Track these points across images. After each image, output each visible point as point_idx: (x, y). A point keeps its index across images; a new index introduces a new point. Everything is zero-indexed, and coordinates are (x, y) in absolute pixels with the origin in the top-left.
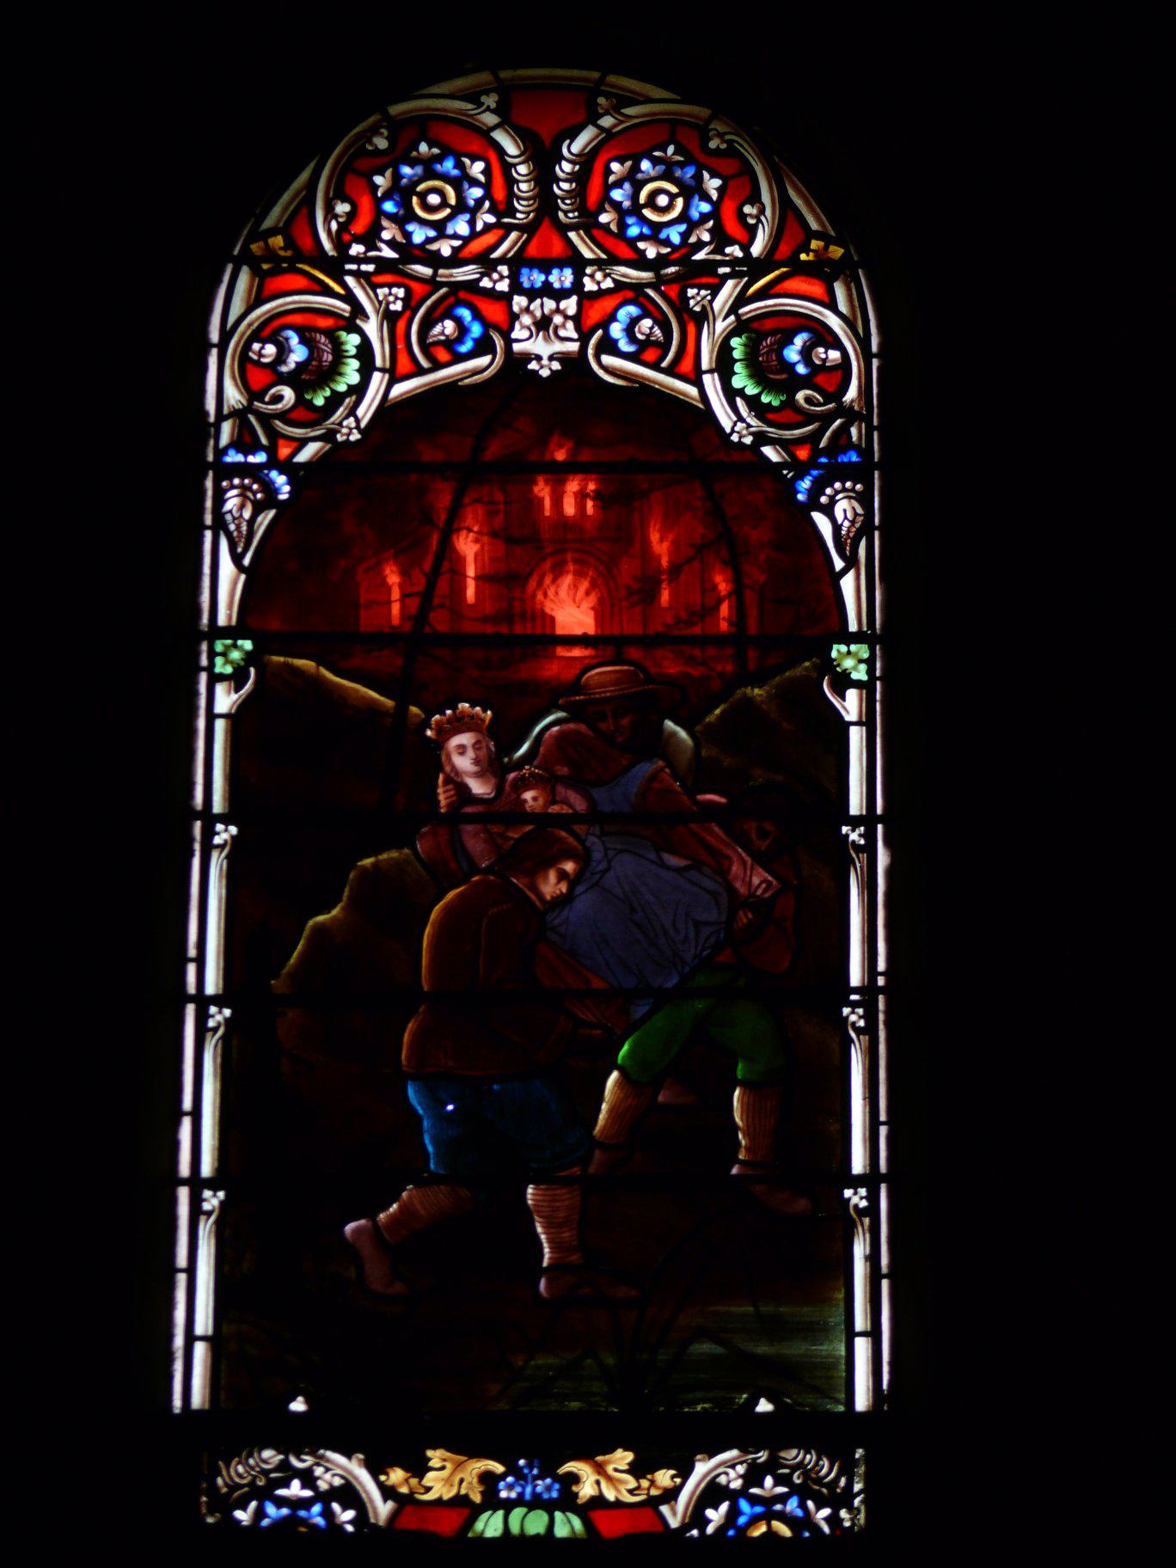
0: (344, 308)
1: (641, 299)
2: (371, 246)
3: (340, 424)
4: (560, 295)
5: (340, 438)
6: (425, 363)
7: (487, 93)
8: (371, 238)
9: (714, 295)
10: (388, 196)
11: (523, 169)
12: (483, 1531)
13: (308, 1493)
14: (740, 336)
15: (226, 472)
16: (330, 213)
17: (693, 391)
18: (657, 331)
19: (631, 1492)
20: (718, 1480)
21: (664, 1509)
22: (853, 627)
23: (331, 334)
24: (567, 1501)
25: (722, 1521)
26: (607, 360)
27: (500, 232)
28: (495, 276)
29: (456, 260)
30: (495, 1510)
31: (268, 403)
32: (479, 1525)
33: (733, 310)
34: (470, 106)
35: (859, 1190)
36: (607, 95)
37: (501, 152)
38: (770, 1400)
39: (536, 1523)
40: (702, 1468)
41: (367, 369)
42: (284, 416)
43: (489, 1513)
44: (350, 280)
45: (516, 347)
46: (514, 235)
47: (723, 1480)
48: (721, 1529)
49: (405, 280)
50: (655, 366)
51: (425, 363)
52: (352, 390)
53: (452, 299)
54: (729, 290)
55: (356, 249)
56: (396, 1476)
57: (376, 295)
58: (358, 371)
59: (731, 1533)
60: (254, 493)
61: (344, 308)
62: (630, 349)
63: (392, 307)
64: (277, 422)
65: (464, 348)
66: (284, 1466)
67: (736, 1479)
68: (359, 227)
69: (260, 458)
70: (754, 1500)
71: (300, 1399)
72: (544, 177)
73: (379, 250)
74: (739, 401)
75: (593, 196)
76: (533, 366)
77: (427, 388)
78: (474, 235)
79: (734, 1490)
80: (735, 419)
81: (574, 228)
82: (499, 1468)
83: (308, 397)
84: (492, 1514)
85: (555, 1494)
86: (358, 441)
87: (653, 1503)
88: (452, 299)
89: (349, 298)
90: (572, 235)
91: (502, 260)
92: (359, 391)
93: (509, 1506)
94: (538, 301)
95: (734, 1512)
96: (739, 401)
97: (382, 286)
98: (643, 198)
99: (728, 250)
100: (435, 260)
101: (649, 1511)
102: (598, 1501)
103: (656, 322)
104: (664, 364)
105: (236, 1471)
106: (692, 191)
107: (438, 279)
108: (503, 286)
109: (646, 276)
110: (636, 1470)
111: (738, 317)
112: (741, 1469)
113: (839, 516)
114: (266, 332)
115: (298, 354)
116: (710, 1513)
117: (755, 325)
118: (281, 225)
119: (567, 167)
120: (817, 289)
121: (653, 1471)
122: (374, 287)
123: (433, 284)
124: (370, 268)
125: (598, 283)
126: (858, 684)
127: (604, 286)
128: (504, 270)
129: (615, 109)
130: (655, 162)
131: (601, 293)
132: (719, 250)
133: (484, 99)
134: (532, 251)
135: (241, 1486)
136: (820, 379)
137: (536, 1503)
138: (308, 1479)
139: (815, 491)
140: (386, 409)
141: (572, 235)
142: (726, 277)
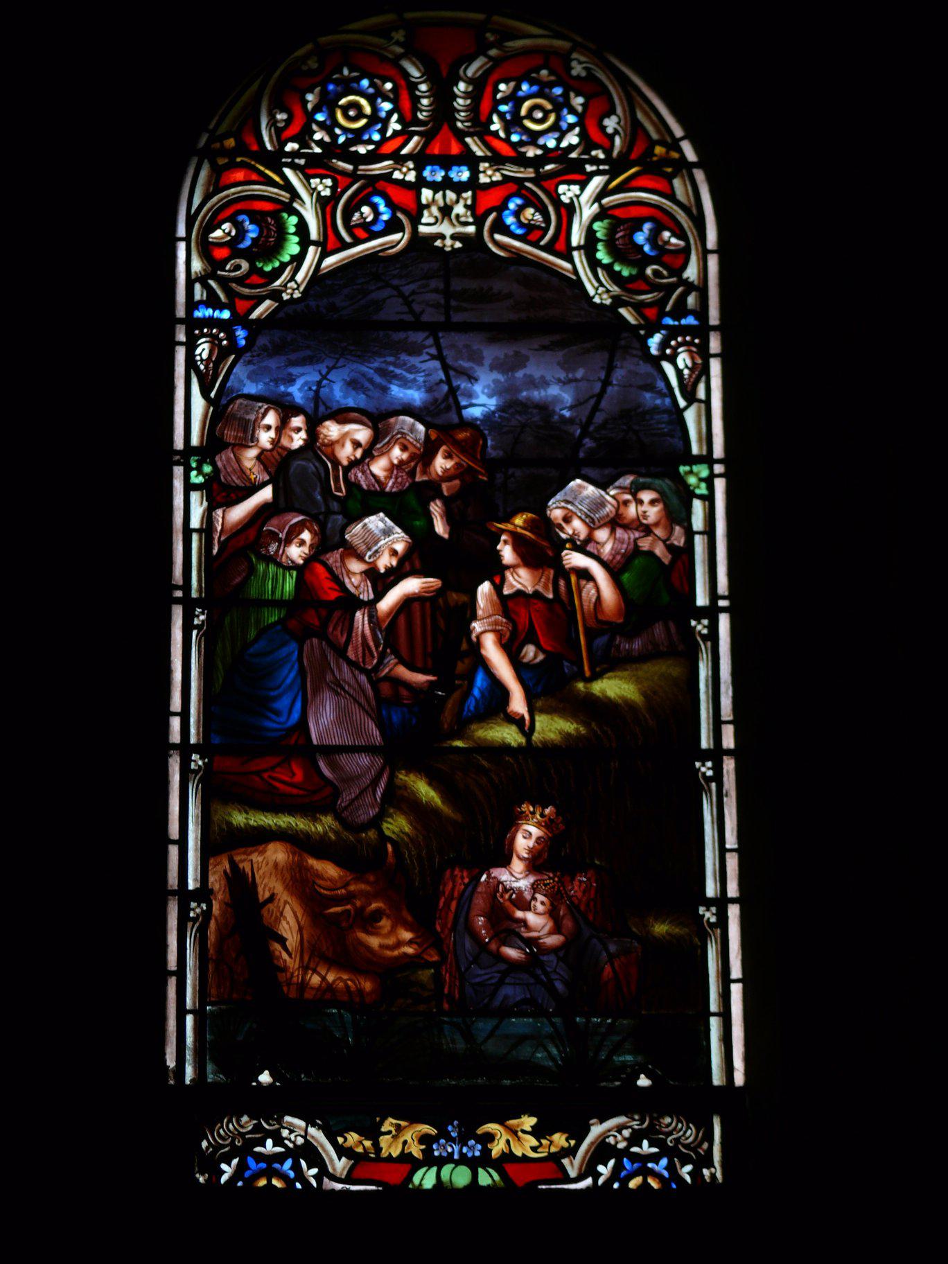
0: (285, 196)
1: (524, 192)
2: (304, 144)
3: (285, 286)
4: (459, 188)
5: (285, 297)
6: (348, 239)
7: (396, 29)
8: (304, 137)
9: (582, 189)
10: (317, 109)
11: (423, 87)
12: (420, 1184)
13: (279, 1149)
14: (602, 220)
15: (192, 324)
16: (273, 122)
17: (568, 266)
18: (538, 217)
19: (534, 1149)
20: (607, 1140)
21: (565, 1161)
22: (695, 450)
23: (276, 216)
24: (485, 1160)
25: (608, 1175)
26: (497, 237)
27: (405, 137)
28: (404, 169)
29: (373, 157)
30: (430, 1167)
31: (229, 271)
32: (416, 1179)
33: (598, 198)
34: (382, 41)
35: (191, 907)
36: (493, 31)
37: (407, 75)
38: (648, 1077)
39: (460, 1177)
40: (596, 1130)
41: (305, 242)
42: (240, 281)
43: (424, 1169)
44: (288, 172)
45: (423, 229)
46: (416, 138)
47: (611, 1140)
48: (610, 1181)
49: (334, 173)
50: (535, 244)
51: (348, 239)
52: (293, 258)
53: (370, 189)
54: (597, 182)
55: (291, 146)
56: (353, 1138)
57: (310, 184)
58: (298, 243)
59: (240, 1184)
60: (222, 340)
61: (285, 196)
62: (519, 231)
63: (323, 194)
64: (234, 285)
65: (378, 228)
66: (258, 1128)
67: (622, 1141)
68: (295, 129)
69: (226, 315)
70: (634, 1158)
71: (267, 1072)
72: (443, 97)
73: (311, 148)
74: (600, 271)
75: (485, 105)
76: (438, 243)
77: (535, 259)
78: (384, 140)
79: (620, 1150)
80: (596, 284)
81: (471, 135)
82: (433, 1131)
83: (259, 265)
84: (427, 1171)
85: (477, 1154)
86: (299, 298)
87: (555, 1159)
88: (370, 189)
89: (288, 187)
90: (468, 140)
91: (409, 157)
92: (298, 259)
93: (440, 1162)
94: (441, 193)
95: (618, 1167)
96: (600, 271)
97: (315, 176)
98: (523, 112)
99: (594, 153)
100: (357, 159)
101: (551, 1165)
102: (508, 1157)
103: (537, 210)
104: (542, 243)
105: (219, 1133)
106: (561, 105)
107: (359, 173)
108: (411, 177)
109: (530, 173)
110: (537, 1132)
111: (601, 206)
112: (626, 1133)
113: (681, 364)
114: (228, 212)
115: (252, 232)
116: (601, 1168)
117: (617, 213)
118: (234, 129)
119: (460, 101)
120: (660, 184)
121: (551, 1134)
122: (308, 178)
123: (354, 177)
124: (302, 162)
125: (490, 177)
126: (701, 497)
127: (494, 179)
128: (411, 165)
129: (498, 44)
130: (372, 85)
131: (493, 184)
132: (587, 151)
133: (393, 34)
134: (436, 149)
135: (224, 1146)
136: (666, 259)
137: (463, 1160)
138: (279, 1141)
139: (664, 344)
140: (317, 278)
141: (468, 140)
142: (591, 175)
